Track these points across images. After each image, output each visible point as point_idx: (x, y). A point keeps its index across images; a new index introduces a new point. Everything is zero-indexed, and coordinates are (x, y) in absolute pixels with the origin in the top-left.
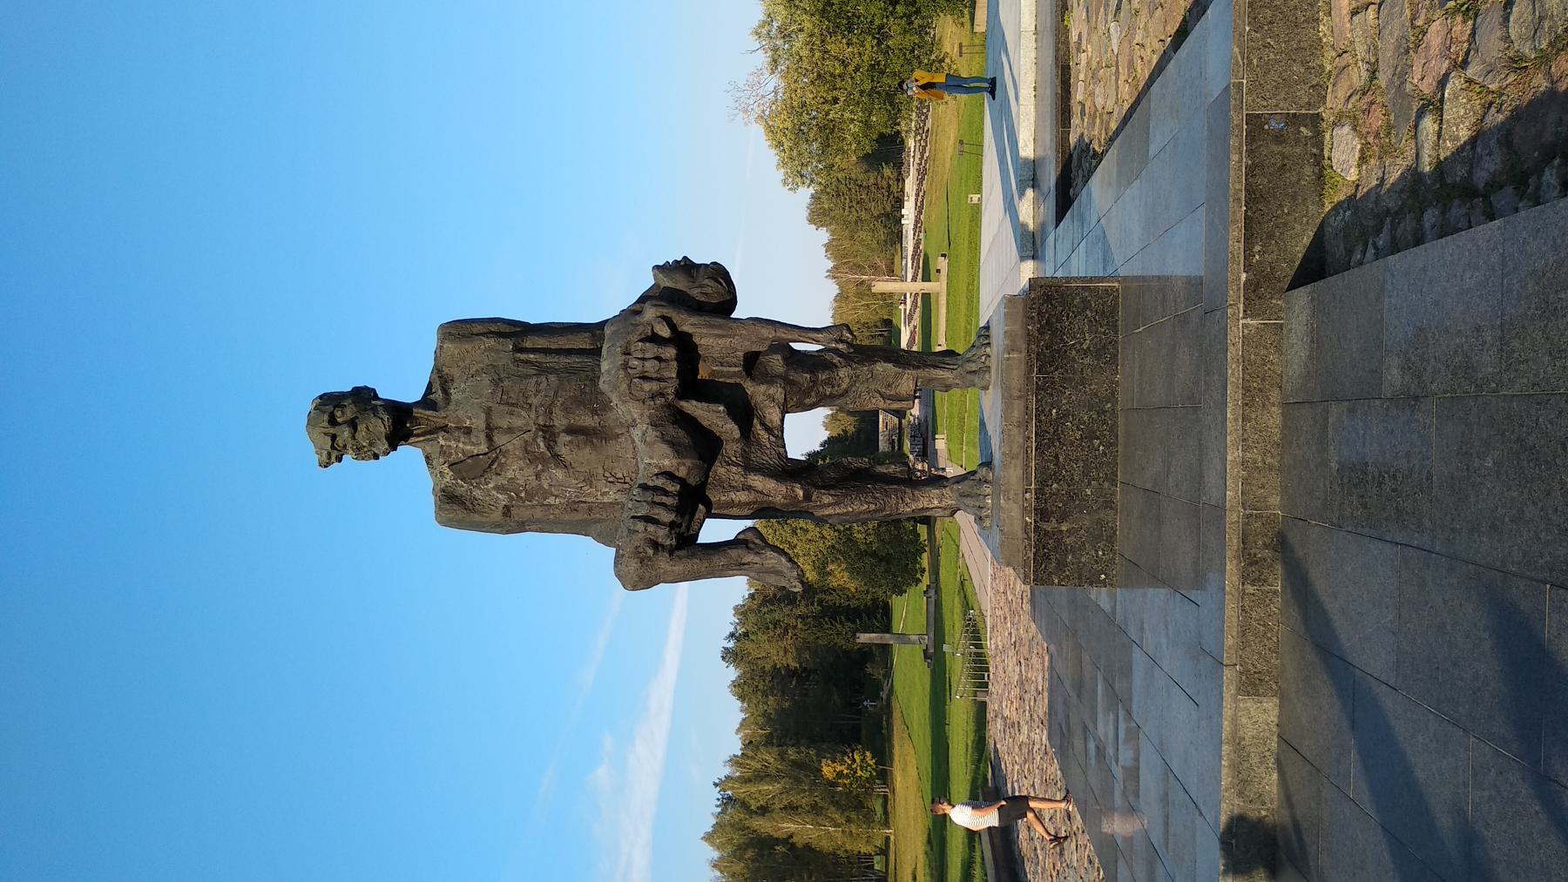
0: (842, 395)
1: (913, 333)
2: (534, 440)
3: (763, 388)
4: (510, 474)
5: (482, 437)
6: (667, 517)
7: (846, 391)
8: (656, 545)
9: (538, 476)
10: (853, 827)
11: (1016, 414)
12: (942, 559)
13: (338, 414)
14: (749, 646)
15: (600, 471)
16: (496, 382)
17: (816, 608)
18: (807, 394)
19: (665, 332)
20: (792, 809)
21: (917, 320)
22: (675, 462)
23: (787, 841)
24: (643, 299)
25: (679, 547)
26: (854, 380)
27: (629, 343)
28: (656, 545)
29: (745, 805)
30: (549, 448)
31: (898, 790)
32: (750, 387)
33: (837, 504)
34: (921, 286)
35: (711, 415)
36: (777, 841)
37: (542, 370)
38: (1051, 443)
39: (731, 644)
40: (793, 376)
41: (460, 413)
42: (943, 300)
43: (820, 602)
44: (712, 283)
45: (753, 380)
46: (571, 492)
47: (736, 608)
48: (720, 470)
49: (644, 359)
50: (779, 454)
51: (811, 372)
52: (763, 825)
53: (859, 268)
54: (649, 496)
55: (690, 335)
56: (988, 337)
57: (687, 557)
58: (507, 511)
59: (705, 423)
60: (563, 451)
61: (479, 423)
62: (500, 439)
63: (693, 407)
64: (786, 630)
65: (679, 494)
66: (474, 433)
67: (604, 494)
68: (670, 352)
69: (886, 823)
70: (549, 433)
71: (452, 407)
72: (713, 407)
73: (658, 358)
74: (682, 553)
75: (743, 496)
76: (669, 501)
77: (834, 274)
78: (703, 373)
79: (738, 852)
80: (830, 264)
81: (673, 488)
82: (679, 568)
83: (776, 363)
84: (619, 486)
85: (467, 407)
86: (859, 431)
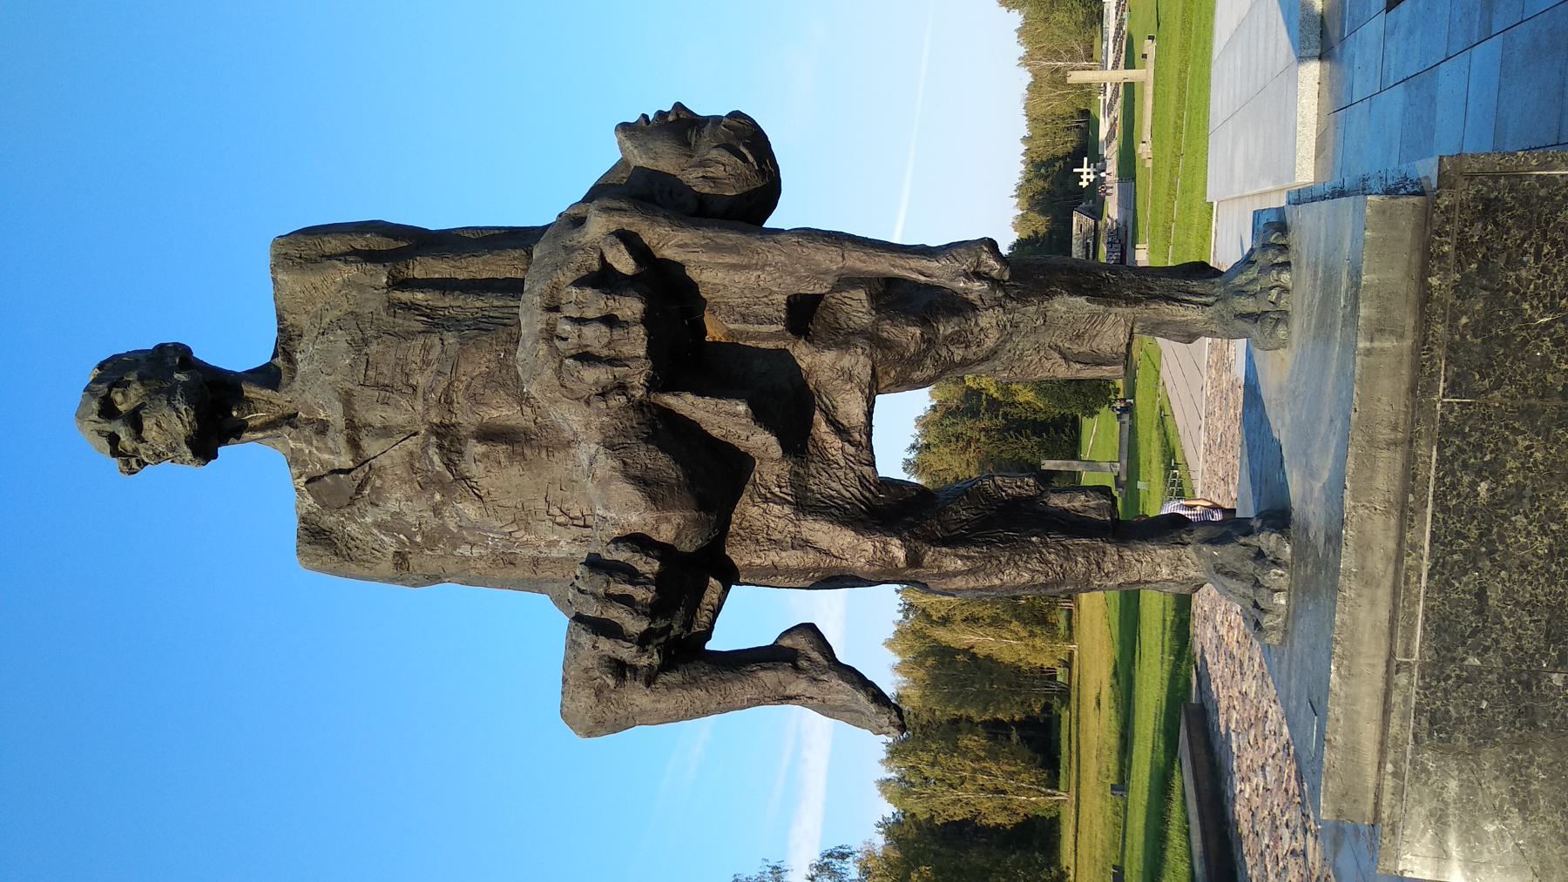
0: (986, 359)
1: (1113, 125)
2: (424, 449)
3: (829, 357)
4: (393, 506)
5: (342, 441)
6: (635, 625)
7: (994, 353)
8: (620, 669)
9: (436, 510)
10: (1038, 642)
11: (1381, 482)
12: (1139, 381)
13: (118, 398)
14: (931, 458)
15: (542, 505)
16: (359, 345)
17: (1001, 421)
18: (916, 361)
19: (624, 263)
20: (972, 620)
21: (1118, 111)
22: (650, 517)
23: (968, 652)
24: (600, 192)
25: (666, 667)
26: (1008, 331)
27: (556, 287)
28: (620, 669)
29: (928, 616)
30: (449, 464)
31: (1083, 607)
32: (805, 355)
33: (970, 572)
34: (1123, 75)
35: (724, 418)
36: (958, 651)
37: (435, 322)
38: (1472, 558)
39: (912, 456)
40: (889, 331)
41: (308, 396)
42: (1149, 90)
43: (1005, 415)
44: (725, 157)
45: (810, 341)
46: (494, 540)
47: (918, 420)
48: (749, 510)
49: (581, 321)
50: (862, 478)
51: (924, 322)
52: (944, 635)
53: (1056, 55)
54: (599, 584)
55: (680, 267)
56: (1284, 248)
57: (682, 686)
58: (401, 559)
59: (715, 433)
60: (475, 470)
61: (334, 414)
62: (371, 447)
63: (687, 404)
64: (969, 443)
65: (660, 580)
66: (331, 433)
67: (551, 544)
68: (631, 307)
69: (1070, 638)
70: (447, 437)
71: (297, 385)
72: (726, 405)
73: (610, 321)
74: (673, 677)
75: (792, 559)
76: (642, 594)
77: (1026, 61)
78: (715, 330)
79: (919, 659)
80: (1022, 51)
81: (648, 566)
82: (667, 703)
83: (857, 308)
84: (576, 531)
85: (315, 391)
86: (1050, 232)
